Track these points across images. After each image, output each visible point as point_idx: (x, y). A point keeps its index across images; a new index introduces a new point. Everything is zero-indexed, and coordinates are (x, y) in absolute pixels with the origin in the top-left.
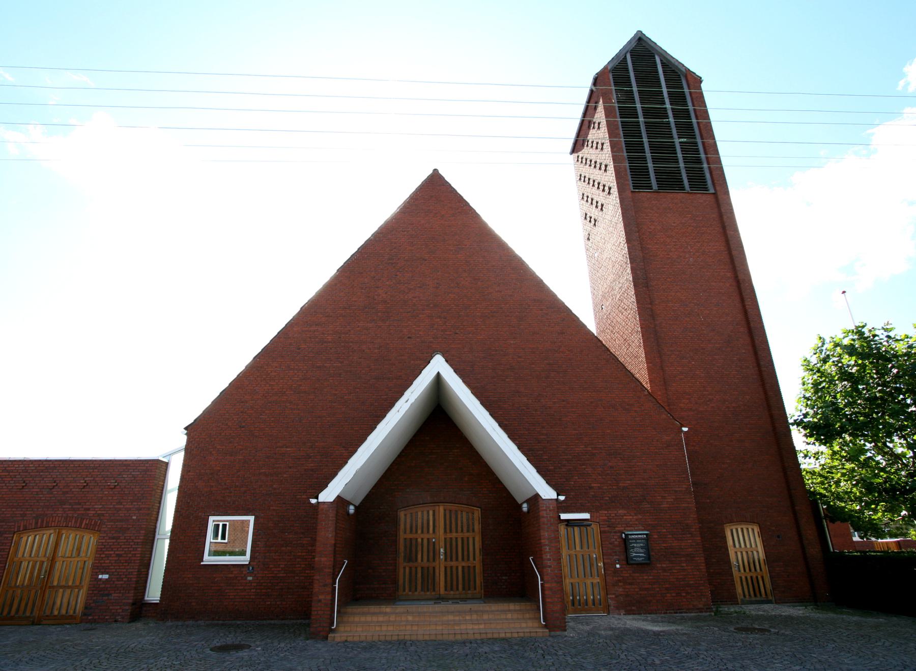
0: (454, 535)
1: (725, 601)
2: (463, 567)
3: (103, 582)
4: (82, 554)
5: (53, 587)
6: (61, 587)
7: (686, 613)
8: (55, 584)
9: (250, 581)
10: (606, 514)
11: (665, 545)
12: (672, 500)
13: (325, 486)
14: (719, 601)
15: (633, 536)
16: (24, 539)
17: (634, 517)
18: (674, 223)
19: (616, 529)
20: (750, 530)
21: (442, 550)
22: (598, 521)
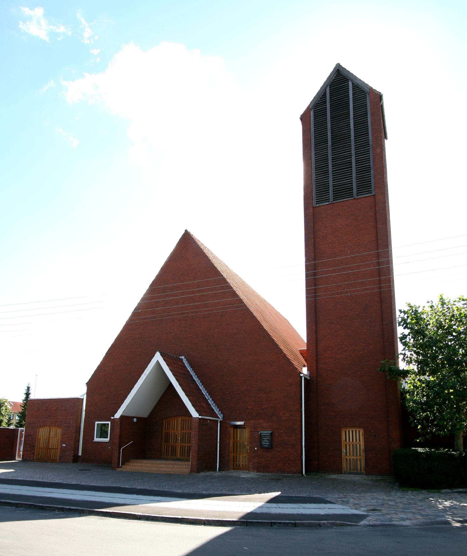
0: (185, 431)
1: (334, 472)
2: (187, 446)
3: (64, 447)
4: (57, 436)
5: (50, 449)
6: (52, 449)
7: (287, 473)
8: (50, 447)
9: (109, 448)
10: (253, 422)
11: (281, 439)
12: (288, 415)
13: (116, 412)
14: (331, 471)
15: (263, 434)
16: (40, 430)
17: (267, 424)
18: (341, 225)
19: (257, 430)
20: (358, 432)
21: (179, 438)
22: (249, 426)
